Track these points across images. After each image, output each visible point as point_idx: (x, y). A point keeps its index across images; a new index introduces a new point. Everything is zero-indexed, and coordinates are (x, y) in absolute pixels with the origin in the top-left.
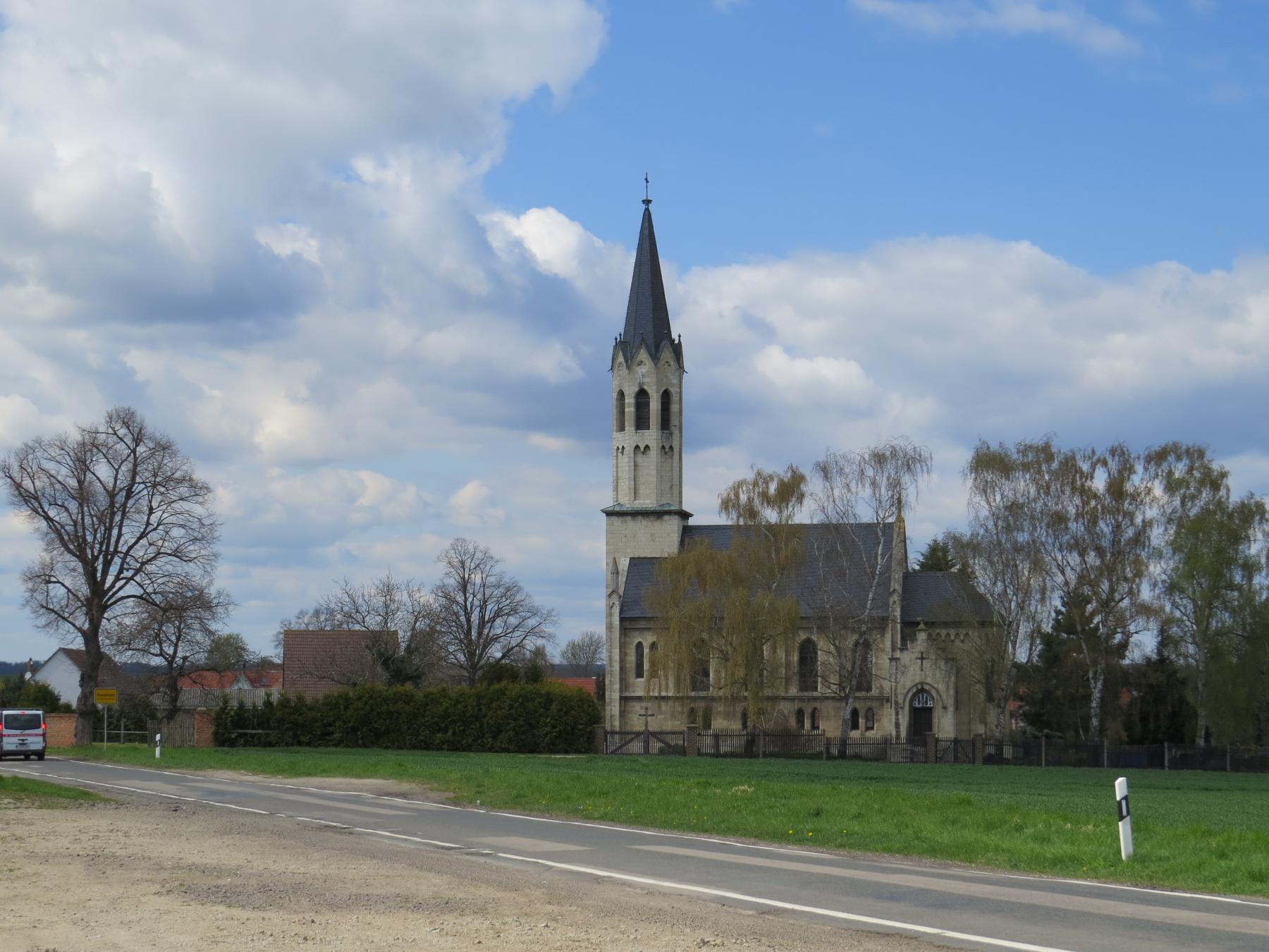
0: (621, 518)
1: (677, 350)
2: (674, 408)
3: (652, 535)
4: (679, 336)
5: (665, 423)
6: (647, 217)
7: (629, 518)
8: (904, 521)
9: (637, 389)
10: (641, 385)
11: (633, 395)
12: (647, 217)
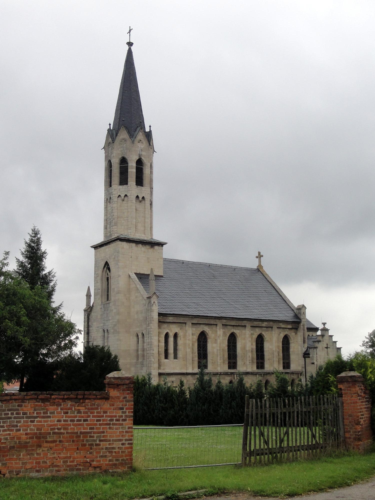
0: (128, 244)
1: (149, 136)
2: (146, 171)
3: (148, 258)
4: (150, 127)
5: (140, 182)
6: (130, 54)
7: (134, 245)
8: (299, 306)
9: (138, 158)
10: (140, 155)
11: (136, 161)
12: (130, 54)
